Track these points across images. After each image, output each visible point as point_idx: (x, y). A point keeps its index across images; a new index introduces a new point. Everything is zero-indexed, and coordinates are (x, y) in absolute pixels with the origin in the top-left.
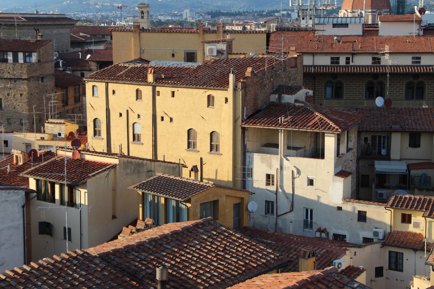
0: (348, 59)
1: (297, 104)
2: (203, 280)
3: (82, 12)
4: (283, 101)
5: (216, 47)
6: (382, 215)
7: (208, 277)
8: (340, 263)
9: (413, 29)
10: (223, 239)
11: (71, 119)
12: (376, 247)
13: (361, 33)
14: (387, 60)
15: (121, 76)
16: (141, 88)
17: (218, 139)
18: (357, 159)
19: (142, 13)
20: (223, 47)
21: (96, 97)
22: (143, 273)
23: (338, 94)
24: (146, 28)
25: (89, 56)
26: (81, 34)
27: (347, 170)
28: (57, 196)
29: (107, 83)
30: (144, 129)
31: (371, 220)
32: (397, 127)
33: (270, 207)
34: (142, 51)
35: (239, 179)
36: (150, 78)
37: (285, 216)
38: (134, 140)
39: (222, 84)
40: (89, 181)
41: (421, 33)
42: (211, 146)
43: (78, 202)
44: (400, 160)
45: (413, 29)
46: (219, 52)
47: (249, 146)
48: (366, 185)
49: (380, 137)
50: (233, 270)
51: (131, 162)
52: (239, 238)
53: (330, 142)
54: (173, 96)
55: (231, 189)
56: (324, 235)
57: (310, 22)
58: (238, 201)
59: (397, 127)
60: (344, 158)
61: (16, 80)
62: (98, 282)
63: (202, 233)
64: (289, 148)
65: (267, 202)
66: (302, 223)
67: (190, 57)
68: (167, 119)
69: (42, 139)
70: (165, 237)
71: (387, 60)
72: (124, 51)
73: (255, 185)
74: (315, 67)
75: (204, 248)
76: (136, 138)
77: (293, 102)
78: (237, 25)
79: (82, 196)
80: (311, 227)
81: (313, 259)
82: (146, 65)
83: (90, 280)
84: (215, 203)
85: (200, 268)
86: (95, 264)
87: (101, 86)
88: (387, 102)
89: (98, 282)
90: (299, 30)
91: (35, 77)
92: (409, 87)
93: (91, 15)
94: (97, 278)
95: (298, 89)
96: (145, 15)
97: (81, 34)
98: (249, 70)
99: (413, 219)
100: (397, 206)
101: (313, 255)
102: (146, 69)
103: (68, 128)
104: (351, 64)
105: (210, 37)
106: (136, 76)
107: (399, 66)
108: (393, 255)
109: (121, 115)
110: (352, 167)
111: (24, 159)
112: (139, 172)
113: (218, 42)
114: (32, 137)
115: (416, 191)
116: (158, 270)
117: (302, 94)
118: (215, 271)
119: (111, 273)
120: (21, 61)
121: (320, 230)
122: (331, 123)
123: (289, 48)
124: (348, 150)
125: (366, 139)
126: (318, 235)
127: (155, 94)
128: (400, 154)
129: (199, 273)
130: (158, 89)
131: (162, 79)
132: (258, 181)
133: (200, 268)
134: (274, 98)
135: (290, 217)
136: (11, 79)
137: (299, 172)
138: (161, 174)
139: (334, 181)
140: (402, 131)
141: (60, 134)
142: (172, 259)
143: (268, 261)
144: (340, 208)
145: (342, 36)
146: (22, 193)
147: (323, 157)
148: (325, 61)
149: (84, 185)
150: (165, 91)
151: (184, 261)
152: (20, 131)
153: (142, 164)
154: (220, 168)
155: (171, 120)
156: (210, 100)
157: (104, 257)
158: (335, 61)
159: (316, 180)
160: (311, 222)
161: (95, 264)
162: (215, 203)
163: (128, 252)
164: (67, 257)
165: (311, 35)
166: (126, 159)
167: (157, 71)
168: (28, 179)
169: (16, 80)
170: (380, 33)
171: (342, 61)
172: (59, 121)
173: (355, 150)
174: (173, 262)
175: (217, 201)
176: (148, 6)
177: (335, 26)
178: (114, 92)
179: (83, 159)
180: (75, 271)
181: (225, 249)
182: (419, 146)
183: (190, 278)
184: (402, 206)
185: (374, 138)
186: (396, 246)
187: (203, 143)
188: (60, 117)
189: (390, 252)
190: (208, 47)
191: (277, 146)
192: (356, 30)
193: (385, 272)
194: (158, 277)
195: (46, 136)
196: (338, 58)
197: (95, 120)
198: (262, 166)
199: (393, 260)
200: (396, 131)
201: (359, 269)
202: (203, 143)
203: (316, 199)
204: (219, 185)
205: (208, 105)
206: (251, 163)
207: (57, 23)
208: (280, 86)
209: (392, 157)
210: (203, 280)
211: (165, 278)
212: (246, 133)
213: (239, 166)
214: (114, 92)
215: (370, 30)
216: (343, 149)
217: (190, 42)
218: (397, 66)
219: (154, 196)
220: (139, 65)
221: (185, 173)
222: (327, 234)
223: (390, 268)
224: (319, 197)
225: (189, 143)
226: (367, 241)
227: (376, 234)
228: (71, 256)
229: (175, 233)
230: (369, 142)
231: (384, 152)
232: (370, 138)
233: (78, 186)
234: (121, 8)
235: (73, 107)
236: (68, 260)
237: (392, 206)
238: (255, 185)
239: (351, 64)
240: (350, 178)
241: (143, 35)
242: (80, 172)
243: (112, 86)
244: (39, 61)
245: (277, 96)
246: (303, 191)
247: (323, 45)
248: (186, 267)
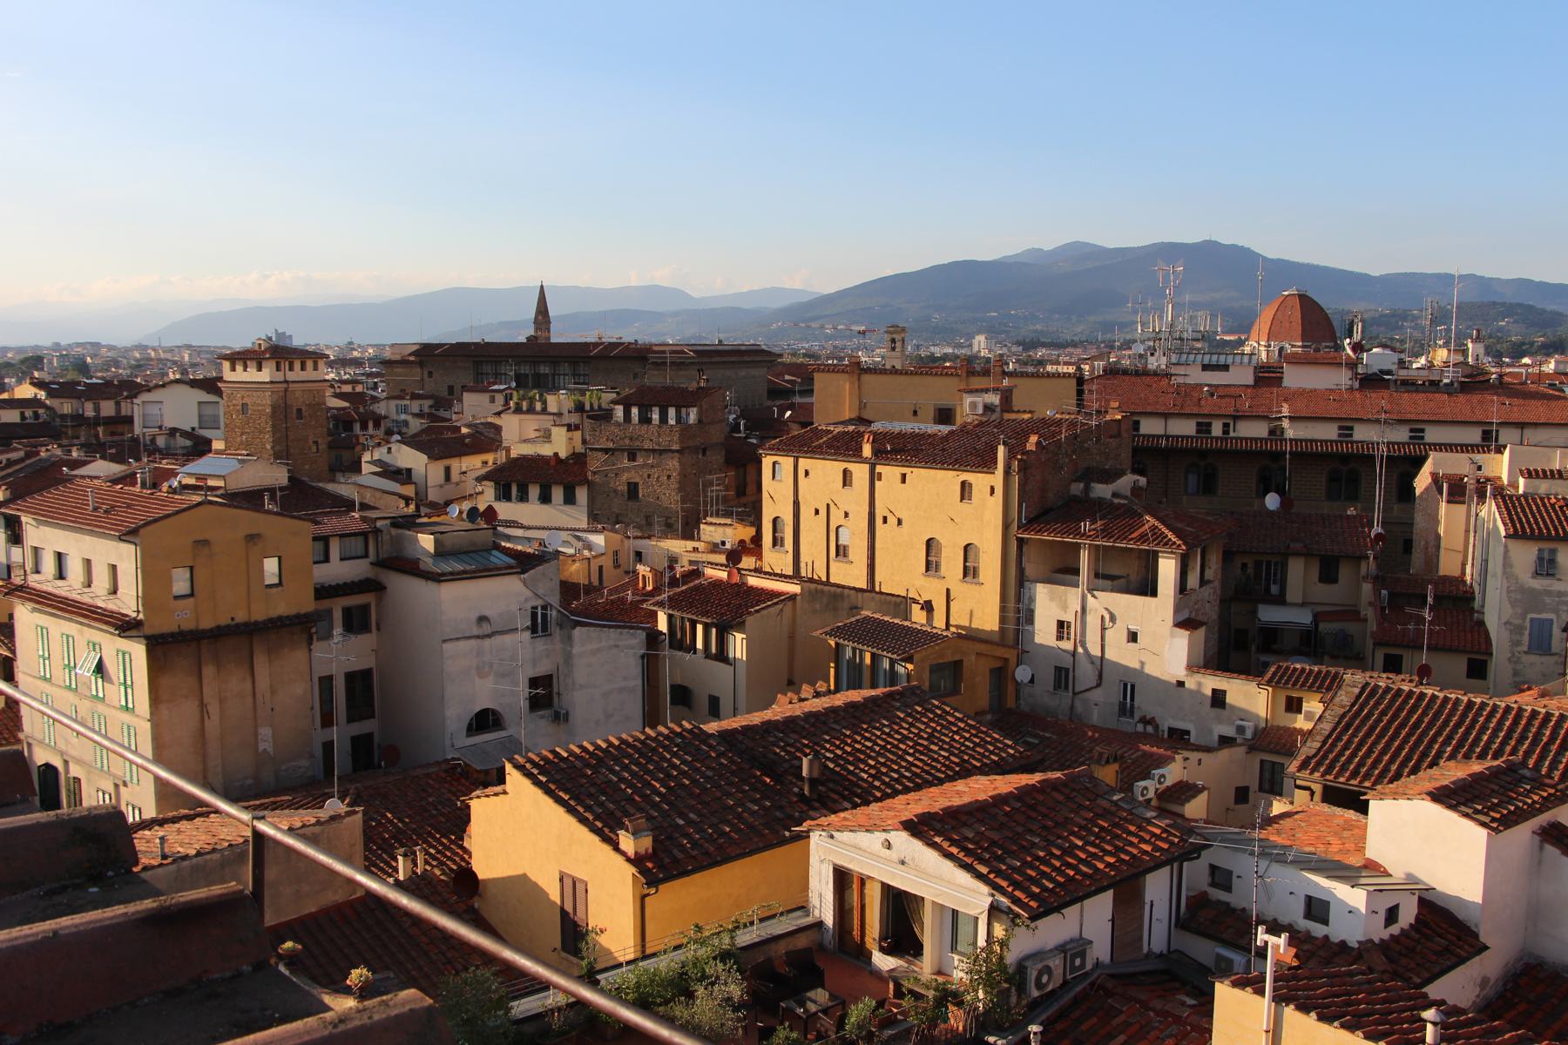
0: (1226, 425)
1: (1116, 501)
2: (883, 782)
3: (801, 340)
4: (1092, 495)
5: (981, 400)
6: (1251, 698)
7: (892, 779)
8: (1163, 776)
9: (1343, 378)
10: (931, 720)
11: (741, 519)
12: (1239, 752)
13: (1251, 381)
14: (1291, 431)
15: (820, 446)
16: (852, 467)
17: (977, 556)
18: (1222, 601)
19: (893, 341)
20: (994, 399)
21: (780, 480)
22: (786, 765)
23: (1208, 485)
24: (898, 367)
25: (788, 413)
26: (787, 377)
27: (1200, 618)
28: (699, 645)
29: (796, 459)
30: (854, 536)
31: (1233, 707)
32: (1298, 546)
33: (1063, 676)
34: (862, 406)
35: (1011, 626)
36: (867, 450)
37: (1087, 695)
38: (837, 555)
39: (985, 463)
40: (750, 620)
41: (1357, 385)
42: (965, 568)
43: (731, 655)
44: (1303, 605)
45: (1343, 378)
46: (988, 408)
47: (1030, 570)
48: (1232, 644)
49: (1268, 563)
50: (939, 771)
51: (822, 591)
52: (960, 720)
53: (1167, 568)
54: (904, 481)
55: (997, 644)
56: (1150, 729)
57: (1164, 360)
58: (997, 664)
59: (1298, 546)
60: (1194, 597)
61: (661, 452)
62: (710, 773)
63: (898, 709)
64: (1097, 576)
65: (1058, 669)
66: (1116, 708)
67: (945, 415)
68: (892, 520)
69: (695, 550)
70: (833, 711)
71: (1291, 431)
72: (833, 403)
73: (1037, 640)
74: (1168, 437)
75: (897, 732)
76: (841, 551)
77: (1109, 496)
78: (1066, 363)
79: (738, 645)
80: (1132, 715)
81: (1116, 767)
82: (862, 429)
83: (698, 769)
84: (958, 665)
85: (883, 764)
86: (710, 746)
87: (786, 463)
88: (1286, 503)
89: (710, 773)
90: (1145, 373)
91: (692, 446)
92: (1333, 479)
93: (815, 346)
94: (708, 768)
95: (1119, 474)
96: (898, 345)
97: (787, 377)
98: (1034, 439)
99: (1305, 707)
100: (1278, 682)
101: (1115, 760)
102: (861, 435)
103: (730, 533)
104: (1232, 434)
105: (977, 382)
106: (843, 446)
107: (1316, 441)
108: (1267, 766)
109: (817, 512)
110: (1212, 612)
111: (655, 581)
112: (836, 609)
113: (987, 391)
114: (676, 546)
115: (1326, 658)
116: (805, 762)
117: (1127, 481)
118: (907, 769)
119: (732, 761)
120: (672, 422)
121: (1145, 721)
122: (1171, 535)
123: (1108, 401)
124: (1203, 582)
125: (1244, 566)
126: (1140, 728)
127: (874, 477)
128: (1300, 596)
129: (879, 771)
130: (879, 469)
131: (887, 452)
132: (1044, 632)
133: (883, 764)
134: (1077, 488)
135: (1096, 695)
136: (654, 451)
137: (1113, 619)
138: (868, 613)
139: (1172, 636)
140: (1307, 554)
141: (723, 543)
142: (838, 747)
143: (1002, 759)
144: (1181, 684)
145: (1218, 386)
146: (642, 635)
147: (1154, 593)
148: (1186, 428)
149: (740, 627)
150: (890, 472)
151: (858, 750)
152: (665, 536)
153: (842, 595)
154: (980, 608)
155: (900, 522)
156: (966, 490)
157: (725, 735)
158: (1204, 428)
159: (1142, 634)
160: (1132, 706)
161: (710, 746)
162: (958, 665)
163: (767, 731)
164: (666, 732)
165: (1165, 382)
166: (813, 586)
167: (879, 440)
168: (655, 614)
169: (661, 452)
170: (1286, 383)
171: (1217, 430)
172: (723, 521)
173: (1217, 584)
174: (839, 752)
175: (961, 661)
176: (903, 330)
177: (1205, 367)
178: (807, 473)
179: (745, 584)
180: (675, 755)
181: (931, 735)
182: (1335, 581)
183: (862, 779)
184: (1287, 682)
185: (1258, 564)
186: (1271, 752)
187: (952, 563)
188: (728, 514)
189: (1262, 762)
190: (968, 400)
191: (1076, 572)
192: (1242, 376)
193: (1251, 796)
194: (805, 773)
195: (700, 545)
196: (1209, 425)
197: (775, 520)
198: (1051, 606)
199: (1267, 775)
200: (1297, 554)
201: (1196, 786)
202: (952, 563)
203: (1137, 666)
204: (970, 636)
205: (962, 499)
206: (1032, 600)
207: (746, 358)
208: (1088, 469)
209: (1289, 598)
210: (883, 782)
211: (816, 774)
212: (1025, 549)
213: (1011, 605)
214: (807, 473)
215: (1267, 376)
216: (1193, 580)
217: (938, 391)
218: (1311, 441)
219: (854, 649)
220: (851, 428)
221: (918, 616)
222: (1156, 727)
223: (1261, 789)
224: (1142, 663)
225: (928, 563)
226: (1225, 741)
227: (1241, 730)
228: (672, 731)
229: (851, 706)
230: (1250, 571)
231: (1274, 589)
232: (1250, 565)
233: (732, 627)
234: (864, 333)
235: (745, 501)
236: (667, 737)
237: (1269, 683)
238: (1037, 640)
239: (1232, 434)
240: (1201, 632)
241: (866, 378)
242: (730, 605)
243: (804, 463)
244: (700, 421)
245: (1082, 485)
246: (1119, 653)
247: (1185, 400)
248: (860, 760)
